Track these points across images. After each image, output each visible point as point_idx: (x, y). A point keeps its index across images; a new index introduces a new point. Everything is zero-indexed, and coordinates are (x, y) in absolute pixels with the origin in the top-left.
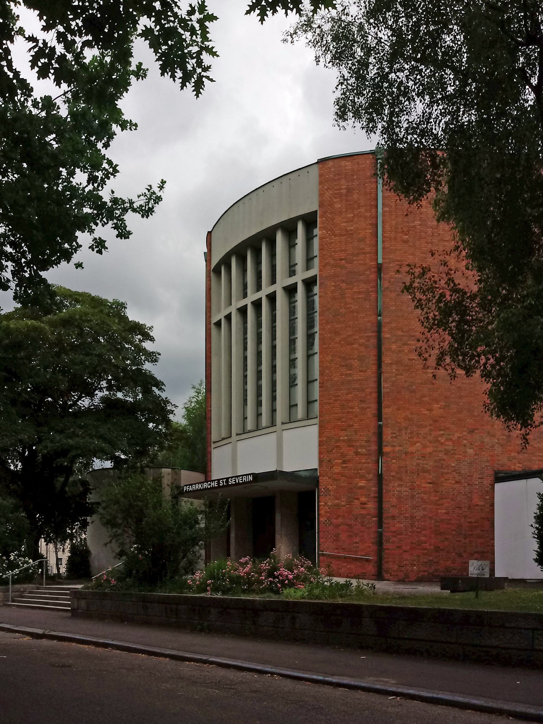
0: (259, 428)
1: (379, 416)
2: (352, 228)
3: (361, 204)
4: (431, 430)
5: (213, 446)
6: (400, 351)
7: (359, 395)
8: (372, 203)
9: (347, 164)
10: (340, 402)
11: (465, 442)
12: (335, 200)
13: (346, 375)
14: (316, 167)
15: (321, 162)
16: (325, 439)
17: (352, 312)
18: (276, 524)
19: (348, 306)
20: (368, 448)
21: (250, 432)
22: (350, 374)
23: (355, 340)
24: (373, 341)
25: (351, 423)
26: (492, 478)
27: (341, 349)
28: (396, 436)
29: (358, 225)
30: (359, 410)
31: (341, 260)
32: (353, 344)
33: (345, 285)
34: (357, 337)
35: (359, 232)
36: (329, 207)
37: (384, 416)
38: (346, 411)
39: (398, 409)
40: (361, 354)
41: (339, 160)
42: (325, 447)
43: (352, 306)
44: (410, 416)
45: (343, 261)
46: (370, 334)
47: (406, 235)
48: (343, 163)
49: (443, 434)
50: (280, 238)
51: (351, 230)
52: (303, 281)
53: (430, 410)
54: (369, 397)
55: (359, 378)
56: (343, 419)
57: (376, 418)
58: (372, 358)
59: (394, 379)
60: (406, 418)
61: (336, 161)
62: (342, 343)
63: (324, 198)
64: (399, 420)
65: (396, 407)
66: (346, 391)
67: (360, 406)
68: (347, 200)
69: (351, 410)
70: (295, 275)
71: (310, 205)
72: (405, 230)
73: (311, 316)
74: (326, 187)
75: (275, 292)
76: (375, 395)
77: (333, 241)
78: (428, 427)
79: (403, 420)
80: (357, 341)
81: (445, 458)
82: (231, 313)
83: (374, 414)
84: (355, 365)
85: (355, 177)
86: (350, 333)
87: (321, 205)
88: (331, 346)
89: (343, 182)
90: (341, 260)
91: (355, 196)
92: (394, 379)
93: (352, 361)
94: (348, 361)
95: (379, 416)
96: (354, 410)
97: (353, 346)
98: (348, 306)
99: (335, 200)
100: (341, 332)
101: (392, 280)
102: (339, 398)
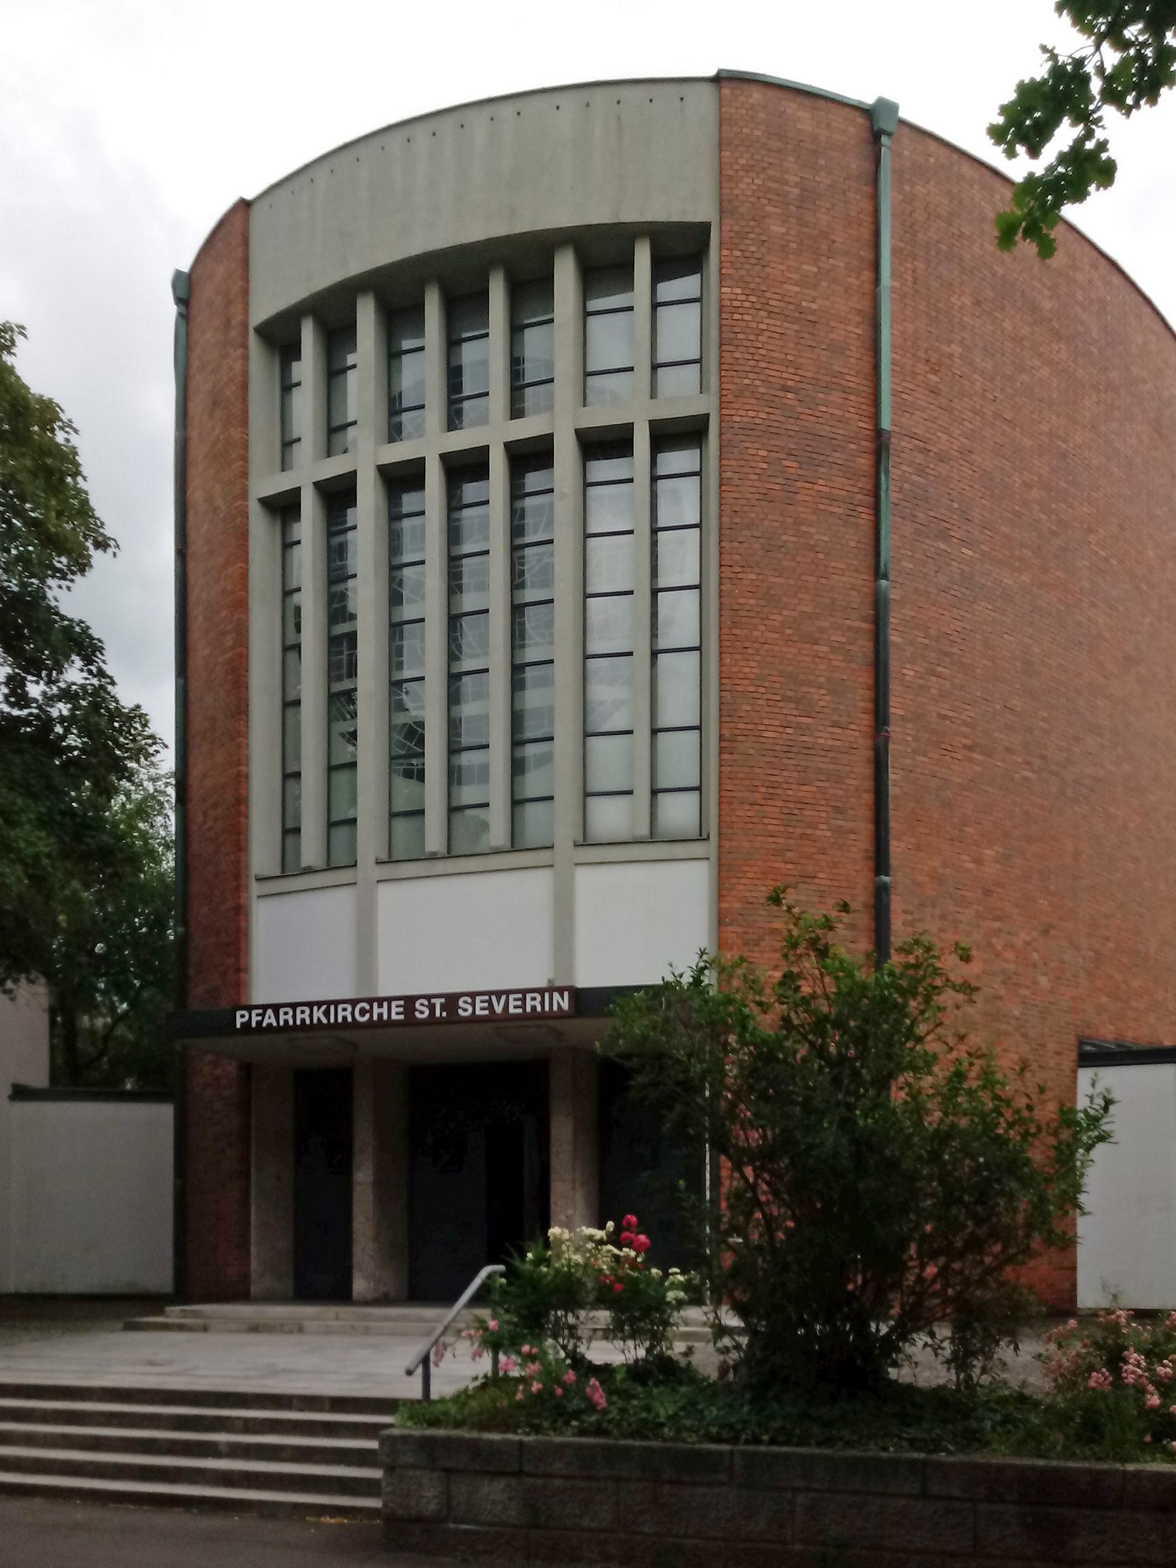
0: (395, 857)
1: (880, 860)
2: (814, 306)
3: (837, 245)
4: (979, 916)
5: (255, 888)
6: (921, 687)
7: (831, 791)
8: (862, 253)
9: (801, 114)
10: (780, 804)
11: (1035, 955)
12: (769, 209)
13: (798, 726)
14: (708, 88)
15: (721, 79)
16: (737, 905)
17: (812, 548)
18: (554, 1149)
19: (804, 528)
20: (852, 946)
21: (309, 871)
22: (808, 727)
23: (822, 630)
24: (863, 647)
25: (810, 868)
26: (1073, 1056)
27: (785, 649)
28: (913, 921)
29: (828, 303)
30: (828, 834)
31: (786, 389)
32: (816, 642)
33: (796, 465)
34: (826, 624)
35: (832, 323)
36: (752, 223)
37: (894, 862)
38: (799, 831)
39: (918, 848)
40: (836, 675)
41: (782, 94)
42: (740, 930)
43: (813, 530)
44: (940, 871)
45: (790, 395)
46: (857, 624)
47: (935, 372)
48: (791, 107)
49: (1000, 930)
50: (366, 316)
51: (813, 312)
52: (508, 446)
53: (978, 861)
54: (853, 800)
55: (830, 742)
56: (789, 854)
57: (871, 864)
58: (861, 691)
59: (908, 761)
60: (935, 877)
61: (771, 93)
62: (788, 631)
63: (736, 192)
64: (920, 879)
65: (913, 840)
66: (795, 774)
67: (833, 822)
68: (803, 223)
69: (809, 831)
70: (422, 435)
71: (685, 199)
72: (933, 360)
73: (457, 563)
74: (742, 161)
75: (353, 475)
76: (868, 798)
77: (764, 327)
78: (975, 907)
79: (927, 879)
80: (825, 636)
81: (1003, 993)
82: (299, 489)
83: (867, 851)
84: (822, 703)
85: (822, 162)
86: (808, 609)
87: (725, 207)
88: (756, 633)
89: (790, 162)
90: (786, 389)
91: (824, 218)
92: (908, 761)
93: (812, 690)
94: (804, 689)
95: (880, 860)
96: (819, 833)
97: (817, 647)
98: (804, 528)
99: (769, 209)
100: (785, 600)
101: (907, 486)
102: (780, 791)
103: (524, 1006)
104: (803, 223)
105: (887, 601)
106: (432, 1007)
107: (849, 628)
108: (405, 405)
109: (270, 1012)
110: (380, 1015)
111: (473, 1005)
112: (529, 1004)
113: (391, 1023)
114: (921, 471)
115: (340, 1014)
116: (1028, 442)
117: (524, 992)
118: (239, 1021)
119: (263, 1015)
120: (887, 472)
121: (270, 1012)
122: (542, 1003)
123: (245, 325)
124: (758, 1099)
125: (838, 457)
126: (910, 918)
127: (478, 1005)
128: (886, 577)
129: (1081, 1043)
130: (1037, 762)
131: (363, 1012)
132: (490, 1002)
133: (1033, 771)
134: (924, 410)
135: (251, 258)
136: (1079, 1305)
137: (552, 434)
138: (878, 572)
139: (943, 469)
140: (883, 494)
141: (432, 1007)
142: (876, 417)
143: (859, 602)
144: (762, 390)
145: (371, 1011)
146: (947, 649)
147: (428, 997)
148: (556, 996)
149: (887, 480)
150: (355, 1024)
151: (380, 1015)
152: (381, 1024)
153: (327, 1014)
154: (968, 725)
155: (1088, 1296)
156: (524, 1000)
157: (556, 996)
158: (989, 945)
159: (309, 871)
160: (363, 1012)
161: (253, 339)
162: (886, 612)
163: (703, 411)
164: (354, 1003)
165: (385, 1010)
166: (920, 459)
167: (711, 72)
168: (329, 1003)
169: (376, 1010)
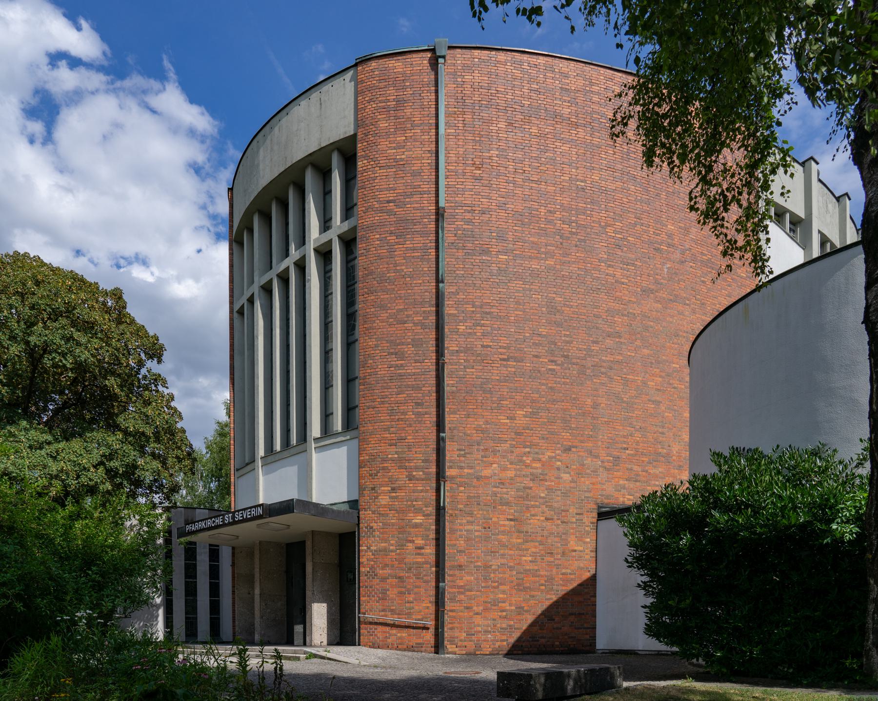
1: (440, 425)
2: (403, 157)
6: (470, 334)
13: (397, 366)
22: (402, 365)
23: (408, 316)
26: (595, 515)
31: (389, 202)
39: (468, 416)
40: (417, 337)
53: (512, 418)
86: (401, 307)
104: (397, 118)
105: (443, 294)
107: (424, 312)
108: (860, 247)
114: (469, 222)
116: (551, 188)
120: (443, 228)
125: (418, 228)
126: (463, 453)
128: (443, 282)
129: (599, 507)
130: (560, 360)
133: (557, 365)
134: (471, 190)
136: (597, 648)
138: (438, 280)
139: (485, 217)
140: (440, 241)
142: (437, 202)
143: (430, 296)
144: (377, 206)
146: (488, 310)
149: (443, 232)
154: (504, 348)
155: (601, 643)
158: (521, 461)
159: (338, 434)
162: (443, 299)
166: (468, 216)
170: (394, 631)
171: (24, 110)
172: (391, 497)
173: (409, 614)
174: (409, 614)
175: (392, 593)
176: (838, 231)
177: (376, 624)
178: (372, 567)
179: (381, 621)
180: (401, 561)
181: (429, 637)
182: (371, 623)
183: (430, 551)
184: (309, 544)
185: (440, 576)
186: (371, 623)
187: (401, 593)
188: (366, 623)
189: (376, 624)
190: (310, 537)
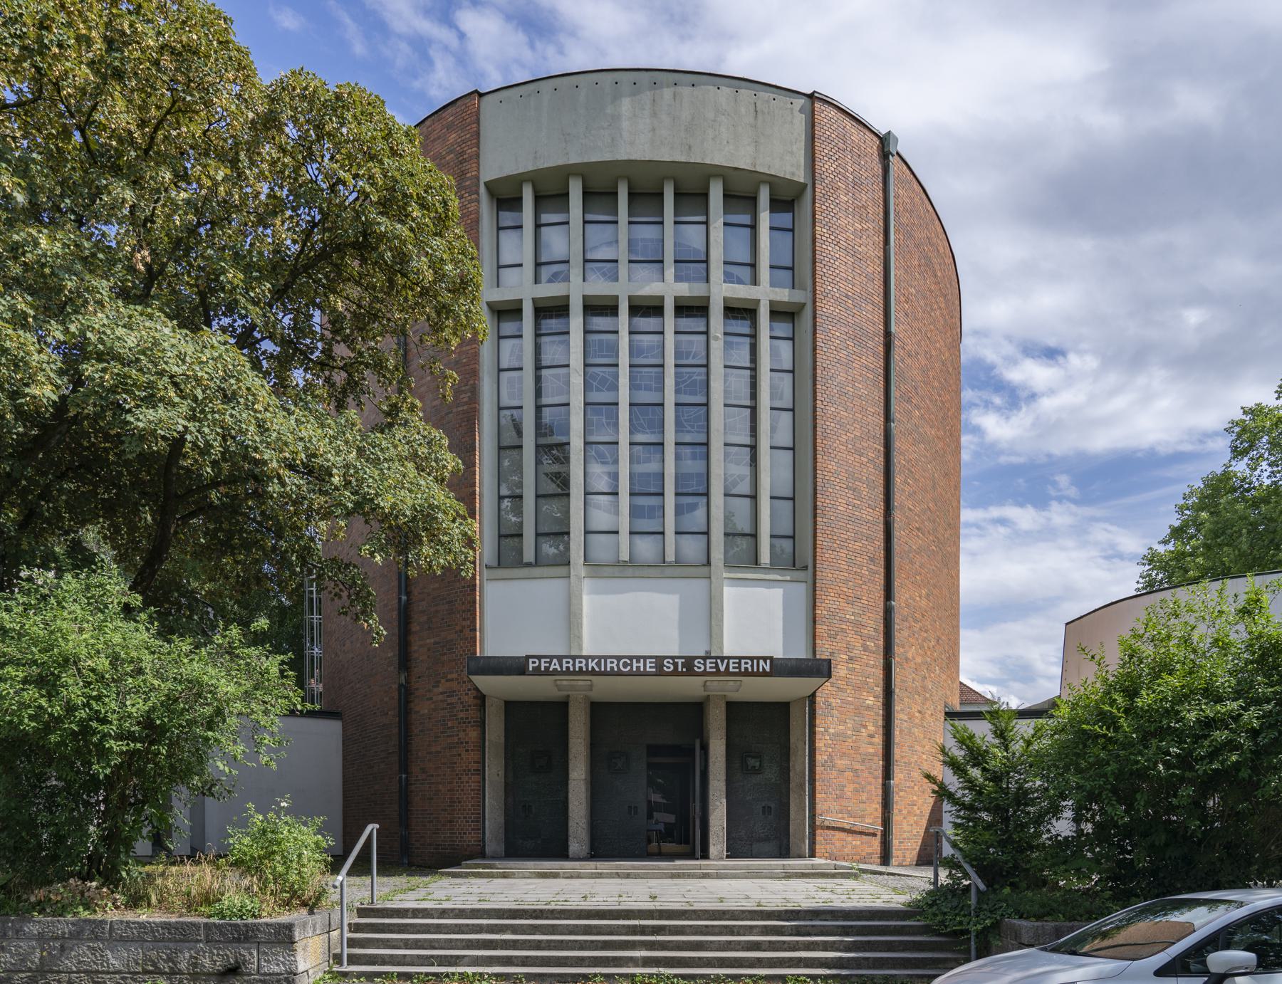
15: (812, 97)
90: (847, 296)
103: (739, 667)
106: (675, 665)
109: (555, 661)
110: (638, 668)
111: (705, 665)
112: (743, 666)
113: (646, 674)
115: (609, 665)
117: (740, 658)
118: (531, 666)
119: (550, 663)
121: (555, 661)
122: (752, 666)
123: (478, 178)
124: (20, 480)
127: (708, 665)
131: (625, 665)
132: (716, 663)
135: (482, 133)
137: (568, 297)
141: (675, 665)
145: (631, 665)
147: (673, 658)
148: (762, 662)
150: (620, 674)
151: (638, 668)
152: (639, 674)
153: (598, 664)
156: (740, 663)
157: (762, 662)
160: (625, 665)
161: (482, 189)
163: (803, 301)
164: (619, 658)
165: (641, 664)
167: (809, 92)
168: (600, 657)
169: (635, 665)
170: (850, 838)
171: (568, 315)
172: (848, 669)
173: (863, 817)
174: (863, 817)
175: (849, 790)
176: (571, 807)
177: (834, 828)
178: (830, 755)
179: (839, 825)
180: (857, 749)
181: (876, 843)
182: (828, 828)
183: (878, 740)
184: (973, 953)
185: (887, 774)
186: (828, 828)
187: (856, 790)
188: (822, 828)
189: (834, 828)
190: (959, 724)
